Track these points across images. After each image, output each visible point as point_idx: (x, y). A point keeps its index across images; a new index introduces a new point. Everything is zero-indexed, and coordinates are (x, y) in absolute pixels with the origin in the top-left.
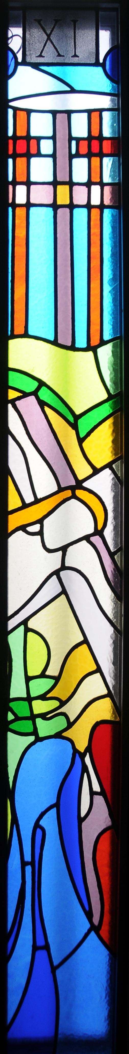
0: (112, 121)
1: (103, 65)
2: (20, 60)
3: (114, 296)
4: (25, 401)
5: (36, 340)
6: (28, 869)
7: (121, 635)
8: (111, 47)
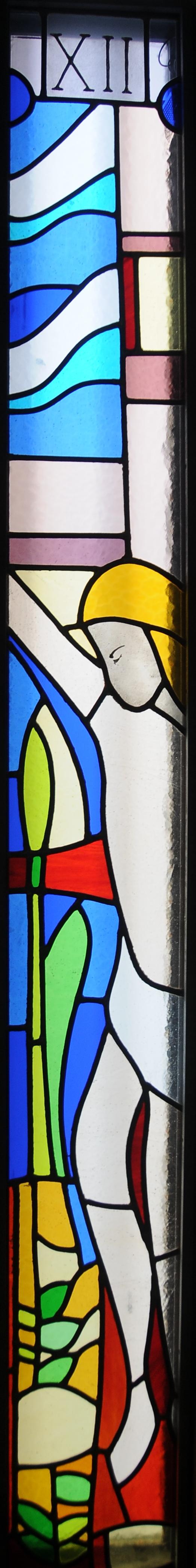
1: (158, 105)
2: (37, 92)
3: (172, 289)
4: (155, 1111)
5: (140, 979)
6: (36, 1035)
7: (184, 590)
8: (170, 80)
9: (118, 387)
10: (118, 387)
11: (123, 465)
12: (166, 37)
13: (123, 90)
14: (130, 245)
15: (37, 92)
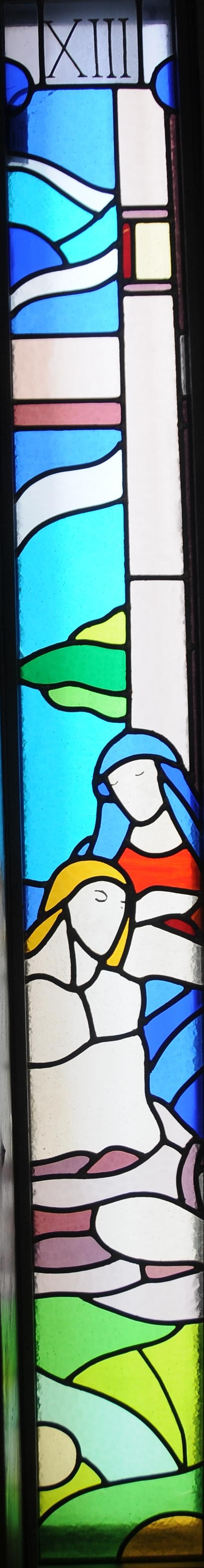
1: (152, 86)
12: (154, 18)
13: (122, 75)
14: (126, 215)
15: (37, 81)
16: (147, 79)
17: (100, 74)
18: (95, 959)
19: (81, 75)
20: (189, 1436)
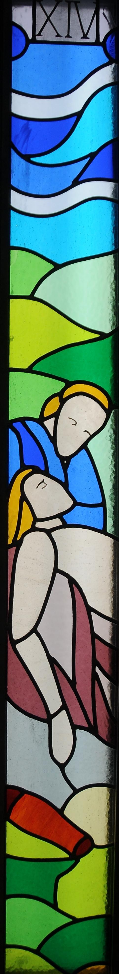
0: (114, 218)
2: (30, 37)
9: (72, 792)
10: (72, 792)
11: (77, 729)
15: (30, 37)
16: (101, 40)
17: (70, 35)
18: (72, 789)
19: (58, 35)
20: (109, 508)
